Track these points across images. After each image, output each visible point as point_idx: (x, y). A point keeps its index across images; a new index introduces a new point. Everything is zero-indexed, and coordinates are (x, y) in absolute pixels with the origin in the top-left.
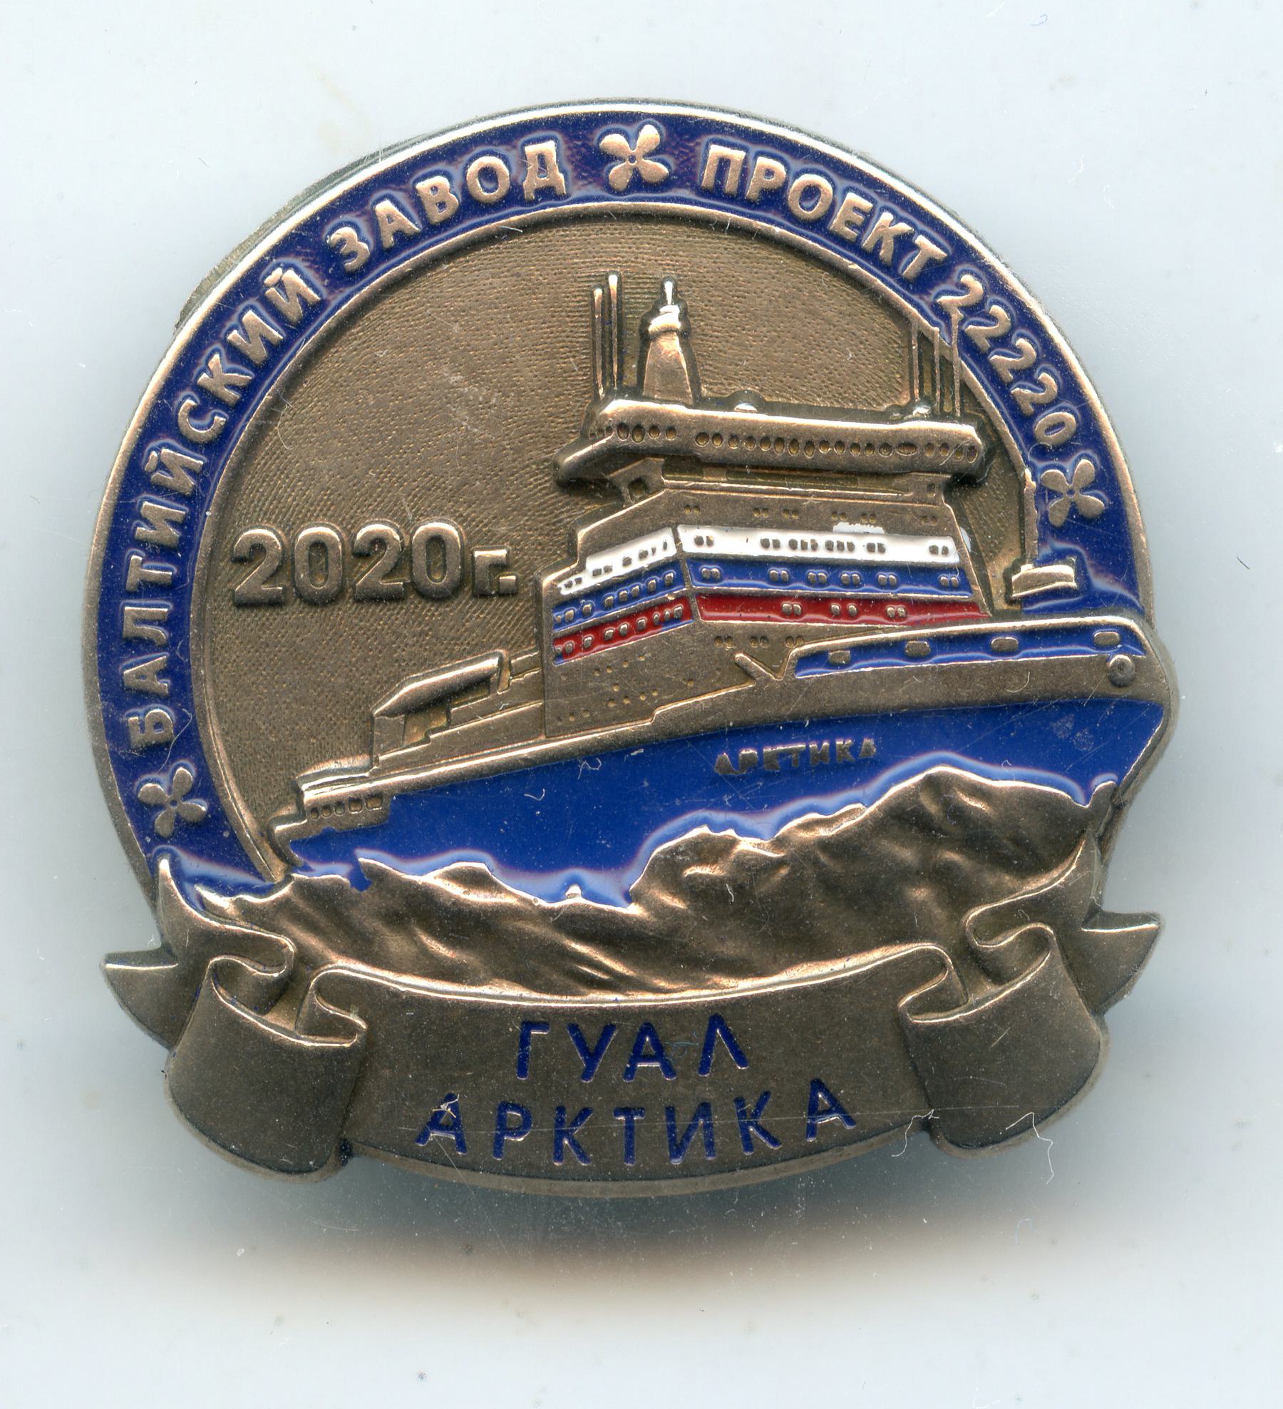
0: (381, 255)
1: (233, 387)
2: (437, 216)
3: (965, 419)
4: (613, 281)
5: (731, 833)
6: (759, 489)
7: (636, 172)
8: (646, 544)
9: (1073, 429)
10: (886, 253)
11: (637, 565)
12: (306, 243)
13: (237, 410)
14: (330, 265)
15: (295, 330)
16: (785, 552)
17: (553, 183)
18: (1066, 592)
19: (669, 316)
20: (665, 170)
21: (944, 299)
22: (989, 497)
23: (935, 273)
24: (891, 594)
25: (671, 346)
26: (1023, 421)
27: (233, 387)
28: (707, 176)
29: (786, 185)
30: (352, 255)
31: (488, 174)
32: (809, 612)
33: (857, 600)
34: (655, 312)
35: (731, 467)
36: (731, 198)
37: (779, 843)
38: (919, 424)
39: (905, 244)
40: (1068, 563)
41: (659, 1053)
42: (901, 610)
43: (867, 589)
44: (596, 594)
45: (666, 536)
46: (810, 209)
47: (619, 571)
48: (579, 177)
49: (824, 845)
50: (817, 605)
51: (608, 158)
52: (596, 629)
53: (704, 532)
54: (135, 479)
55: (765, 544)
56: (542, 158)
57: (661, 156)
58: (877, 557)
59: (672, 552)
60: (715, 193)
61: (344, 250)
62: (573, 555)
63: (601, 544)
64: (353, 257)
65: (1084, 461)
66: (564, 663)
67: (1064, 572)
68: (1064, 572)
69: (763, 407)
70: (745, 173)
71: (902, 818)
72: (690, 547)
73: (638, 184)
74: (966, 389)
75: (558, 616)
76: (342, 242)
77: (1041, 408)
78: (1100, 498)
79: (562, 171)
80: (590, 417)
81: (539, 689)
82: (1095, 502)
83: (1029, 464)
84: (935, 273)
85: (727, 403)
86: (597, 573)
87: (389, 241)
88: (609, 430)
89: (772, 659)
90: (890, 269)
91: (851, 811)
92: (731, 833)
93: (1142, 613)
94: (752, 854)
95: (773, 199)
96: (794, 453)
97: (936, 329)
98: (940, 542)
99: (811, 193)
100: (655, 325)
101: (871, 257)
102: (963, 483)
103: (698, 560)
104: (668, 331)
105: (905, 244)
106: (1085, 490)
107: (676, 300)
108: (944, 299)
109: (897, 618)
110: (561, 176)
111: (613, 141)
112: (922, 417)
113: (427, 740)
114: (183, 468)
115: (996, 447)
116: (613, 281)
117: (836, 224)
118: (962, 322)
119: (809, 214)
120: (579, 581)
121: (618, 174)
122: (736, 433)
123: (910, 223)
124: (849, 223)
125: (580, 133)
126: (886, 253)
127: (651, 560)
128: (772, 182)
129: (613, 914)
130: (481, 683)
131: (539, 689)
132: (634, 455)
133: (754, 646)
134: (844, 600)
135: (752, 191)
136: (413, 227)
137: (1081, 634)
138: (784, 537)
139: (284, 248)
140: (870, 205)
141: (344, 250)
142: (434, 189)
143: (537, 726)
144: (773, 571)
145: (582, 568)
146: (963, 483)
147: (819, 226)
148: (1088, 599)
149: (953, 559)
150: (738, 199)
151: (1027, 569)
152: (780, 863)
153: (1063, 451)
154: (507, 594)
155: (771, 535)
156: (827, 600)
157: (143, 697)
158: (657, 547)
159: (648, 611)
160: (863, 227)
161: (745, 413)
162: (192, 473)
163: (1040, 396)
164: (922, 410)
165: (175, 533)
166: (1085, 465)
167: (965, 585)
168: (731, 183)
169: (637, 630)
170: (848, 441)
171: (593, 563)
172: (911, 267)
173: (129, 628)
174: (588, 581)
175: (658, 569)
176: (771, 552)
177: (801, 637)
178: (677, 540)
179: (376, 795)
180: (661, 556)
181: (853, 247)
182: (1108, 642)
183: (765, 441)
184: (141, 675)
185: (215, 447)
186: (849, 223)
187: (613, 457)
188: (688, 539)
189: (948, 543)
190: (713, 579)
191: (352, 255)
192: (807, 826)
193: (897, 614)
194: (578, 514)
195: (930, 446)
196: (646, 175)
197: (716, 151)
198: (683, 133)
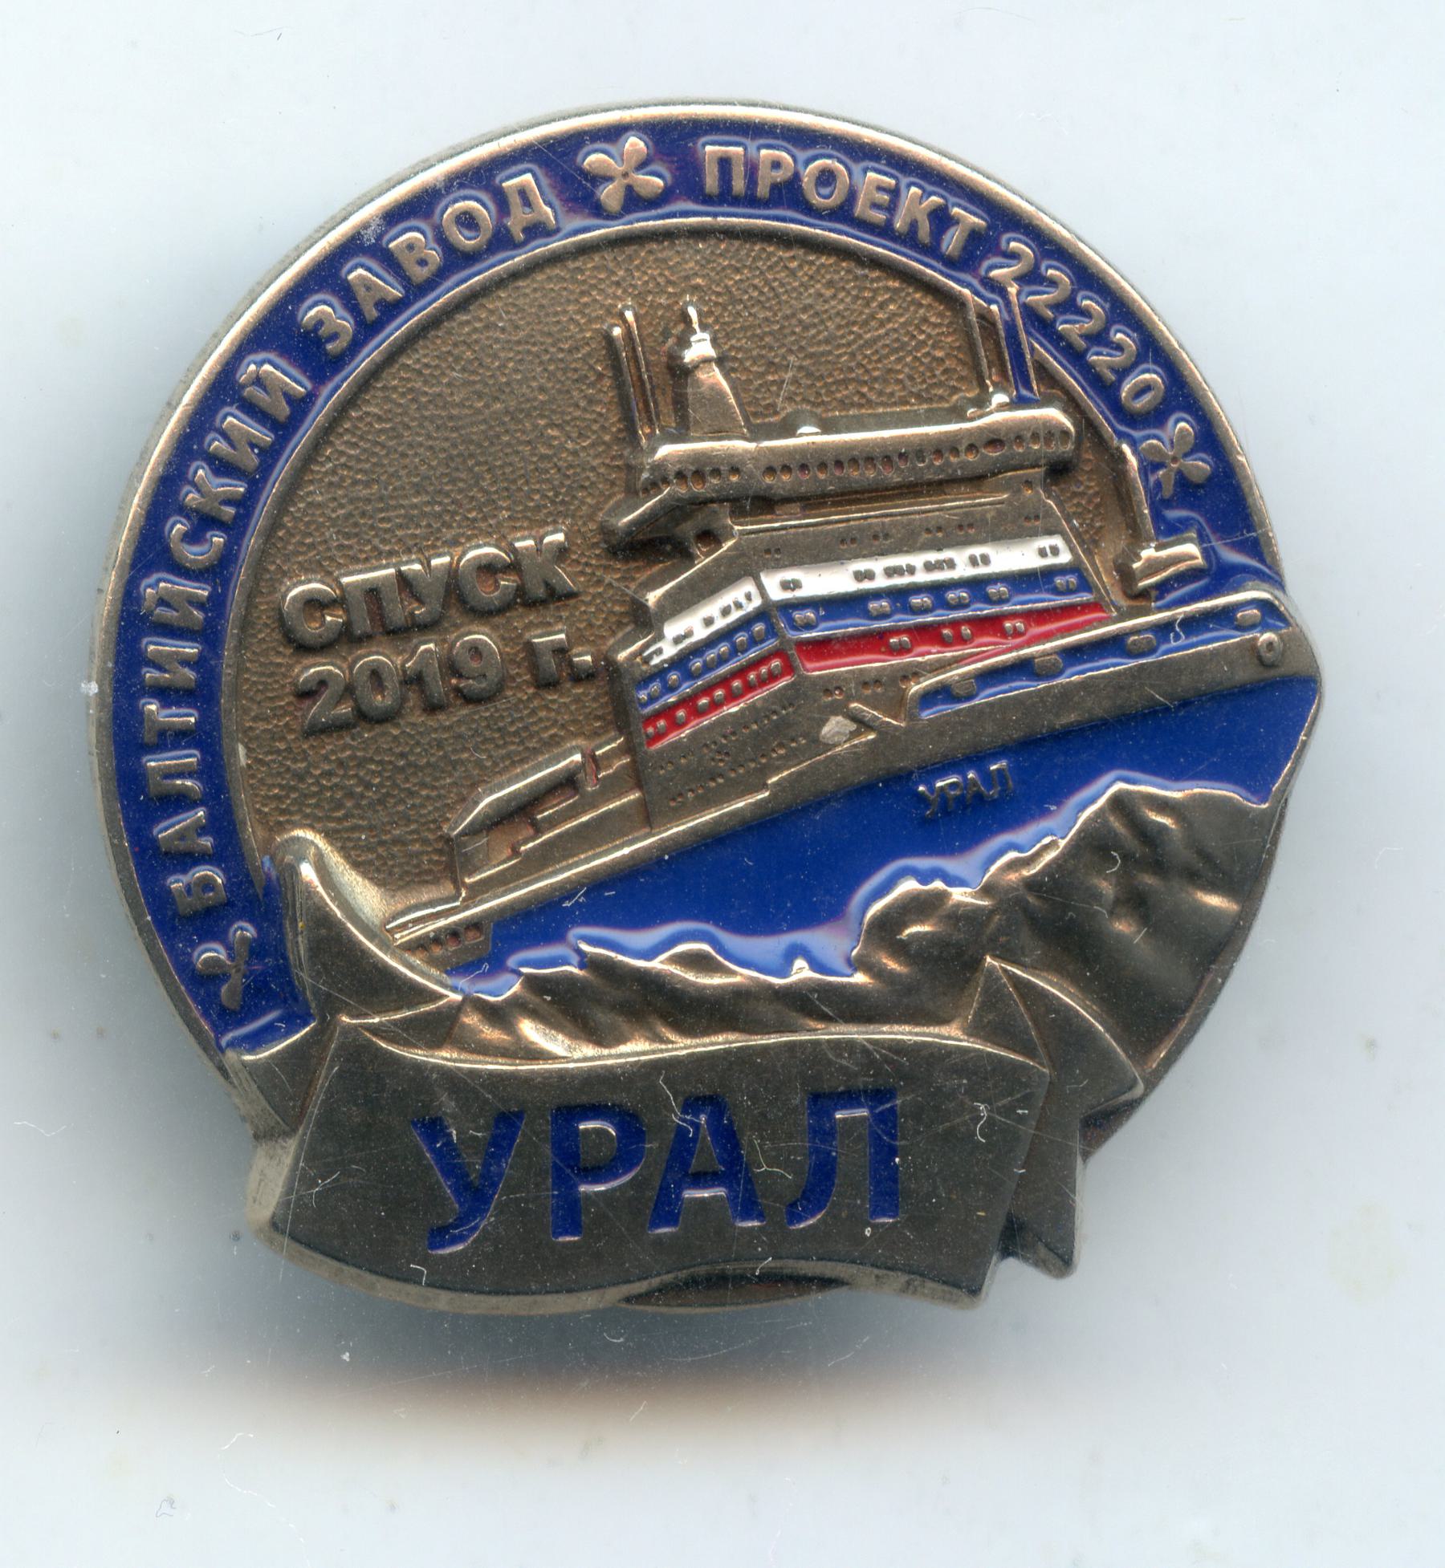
0: (367, 330)
1: (228, 502)
2: (420, 274)
3: (1045, 402)
4: (629, 315)
5: (938, 885)
6: (838, 519)
7: (629, 189)
8: (727, 598)
9: (1161, 394)
10: (924, 232)
11: (720, 623)
12: (278, 330)
13: (235, 529)
14: (313, 354)
15: (284, 430)
16: (881, 582)
17: (543, 219)
18: (1194, 574)
19: (700, 347)
20: (659, 182)
21: (994, 273)
22: (1087, 483)
23: (980, 246)
24: (1006, 608)
25: (714, 377)
26: (1107, 390)
27: (228, 502)
28: (711, 183)
29: (796, 177)
30: (334, 337)
31: (468, 221)
32: (919, 645)
33: (969, 621)
34: (684, 342)
35: (811, 502)
36: (736, 201)
37: (987, 890)
38: (999, 411)
39: (941, 219)
40: (1190, 540)
41: (732, 1169)
42: (1020, 625)
43: (980, 608)
44: (680, 662)
45: (749, 586)
46: (828, 197)
47: (701, 634)
48: (571, 210)
49: (1031, 884)
50: (928, 634)
51: (600, 178)
52: (688, 702)
53: (790, 574)
54: (132, 624)
55: (1042, 553)
56: (523, 193)
57: (649, 169)
58: (982, 570)
59: (757, 602)
60: (725, 197)
61: (323, 331)
62: (646, 622)
63: (679, 603)
64: (333, 340)
65: (1182, 424)
66: (659, 745)
67: (1190, 550)
68: (1190, 550)
69: (827, 427)
70: (752, 170)
71: (1094, 845)
72: (776, 594)
73: (634, 201)
74: (1042, 369)
75: (643, 695)
76: (320, 323)
77: (1123, 373)
78: (1203, 460)
79: (549, 204)
80: (631, 469)
81: (637, 776)
82: (1200, 466)
83: (1121, 435)
84: (980, 246)
85: (788, 428)
86: (677, 640)
87: (372, 313)
88: (666, 481)
89: (896, 703)
90: (931, 251)
91: (1043, 843)
92: (938, 885)
93: (1275, 579)
94: (967, 905)
95: (789, 194)
96: (871, 474)
97: (994, 307)
98: (1046, 542)
99: (826, 178)
100: (689, 356)
101: (909, 239)
102: (1059, 471)
103: (787, 607)
104: (707, 361)
105: (941, 219)
106: (1186, 455)
107: (704, 327)
108: (994, 273)
109: (1017, 633)
110: (548, 210)
111: (594, 159)
112: (1002, 407)
113: (515, 852)
114: (191, 603)
115: (1087, 424)
116: (629, 315)
117: (860, 209)
118: (1019, 294)
119: (830, 202)
120: (659, 651)
121: (609, 195)
122: (804, 461)
123: (942, 197)
124: (876, 206)
125: (558, 158)
126: (924, 232)
127: (735, 615)
128: (780, 176)
129: (844, 986)
130: (568, 782)
131: (637, 776)
132: (701, 503)
133: (868, 692)
134: (955, 624)
135: (763, 190)
136: (395, 292)
137: (1225, 617)
138: (878, 565)
139: (257, 339)
140: (893, 182)
141: (323, 331)
142: (410, 247)
143: (647, 816)
144: (873, 605)
145: (660, 637)
146: (1059, 471)
147: (843, 214)
148: (1219, 577)
149: (1065, 557)
150: (751, 200)
151: (1148, 553)
152: (992, 912)
153: (1156, 417)
154: (582, 676)
155: (862, 565)
156: (884, 635)
157: (186, 860)
158: (739, 598)
159: (741, 672)
160: (891, 208)
161: (809, 436)
162: (200, 605)
163: (1119, 359)
164: (1000, 398)
165: (191, 675)
166: (1182, 426)
167: (1085, 585)
168: (739, 185)
169: (732, 697)
170: (777, 465)
171: (672, 629)
172: (952, 241)
173: (156, 786)
174: (669, 650)
175: (745, 623)
176: (867, 585)
177: (915, 673)
178: (761, 587)
179: (474, 925)
180: (750, 607)
181: (884, 231)
182: (1250, 622)
183: (699, 475)
184: (181, 836)
185: (218, 572)
186: (876, 206)
187: (677, 510)
188: (774, 585)
189: (1057, 541)
190: (809, 626)
191: (334, 337)
192: (1013, 865)
193: (1015, 628)
194: (642, 577)
195: (1019, 438)
196: (644, 192)
197: (712, 150)
198: (673, 139)
